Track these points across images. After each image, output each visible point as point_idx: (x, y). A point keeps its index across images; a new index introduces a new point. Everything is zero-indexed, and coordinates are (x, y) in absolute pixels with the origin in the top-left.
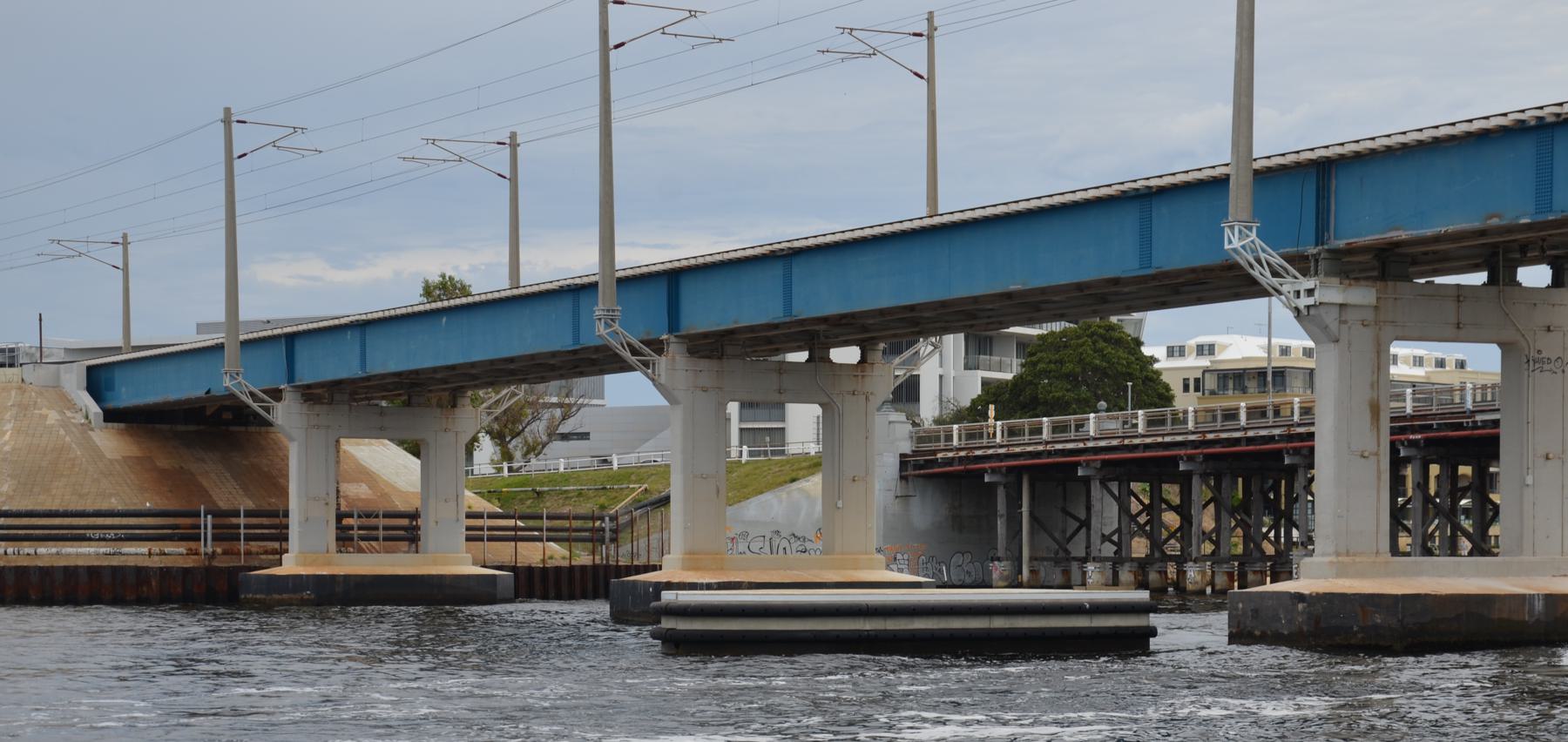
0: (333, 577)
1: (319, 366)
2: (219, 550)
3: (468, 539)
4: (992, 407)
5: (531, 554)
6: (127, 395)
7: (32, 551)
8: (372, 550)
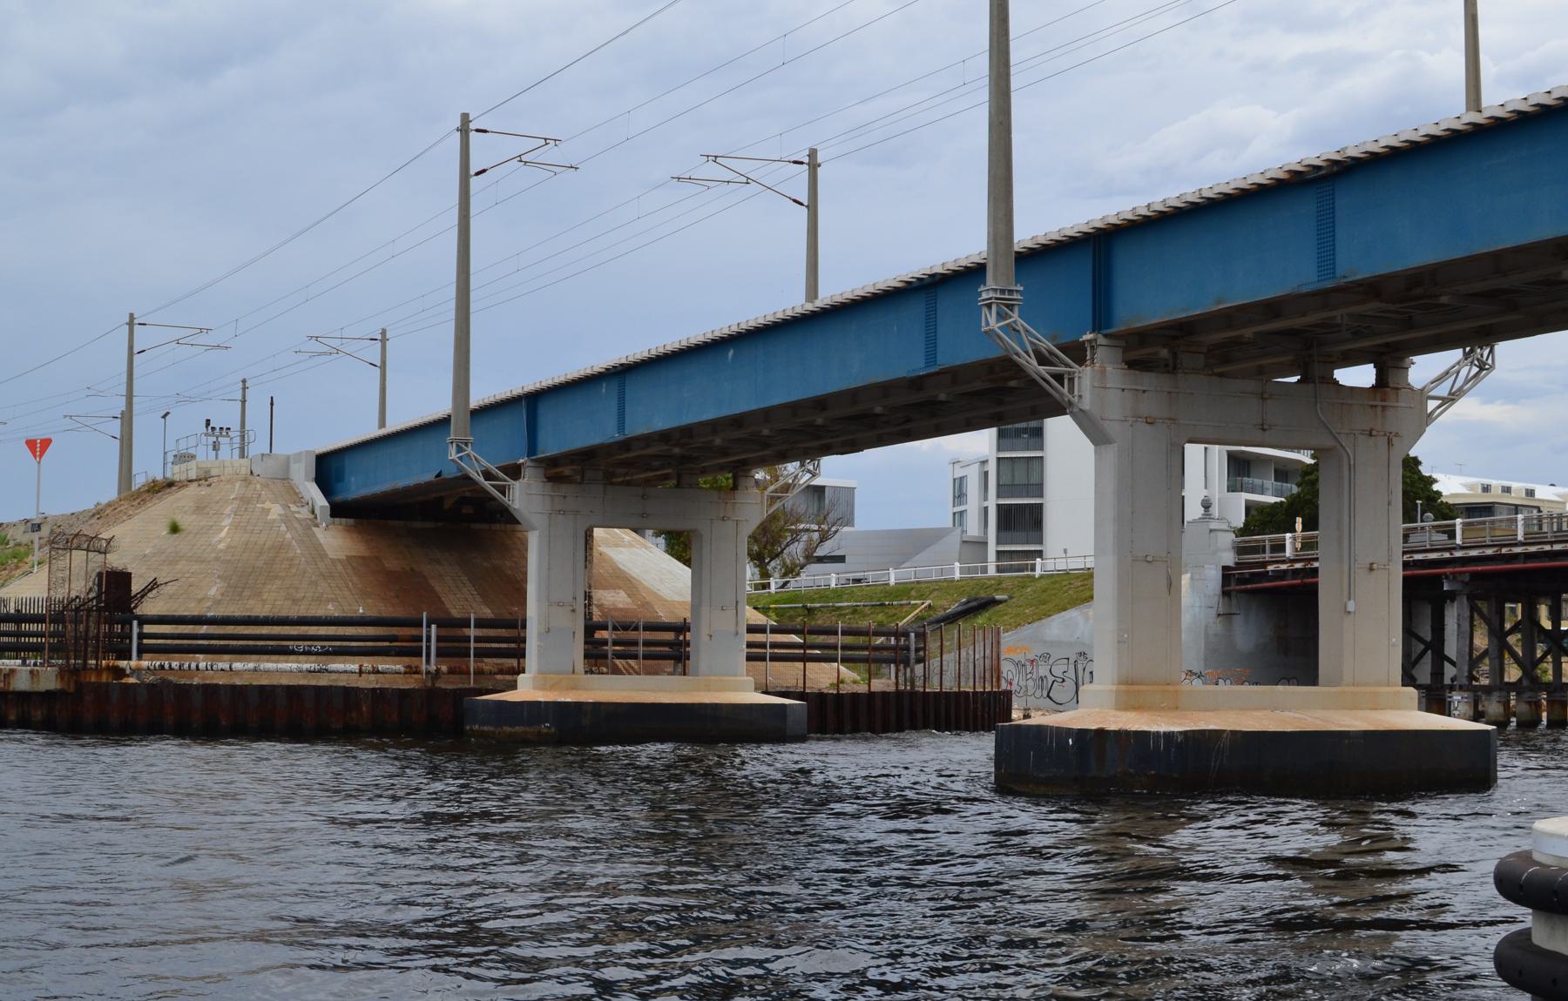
0: (578, 706)
1: (568, 432)
2: (444, 668)
3: (750, 658)
4: (1299, 520)
5: (823, 676)
6: (357, 487)
7: (226, 666)
8: (630, 671)
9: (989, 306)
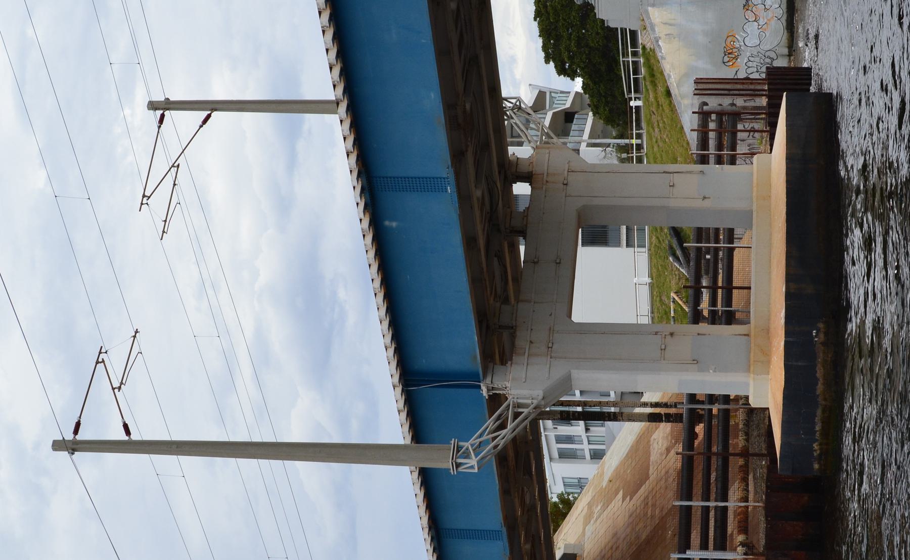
0: (789, 296)
2: (741, 538)
9: (458, 465)
